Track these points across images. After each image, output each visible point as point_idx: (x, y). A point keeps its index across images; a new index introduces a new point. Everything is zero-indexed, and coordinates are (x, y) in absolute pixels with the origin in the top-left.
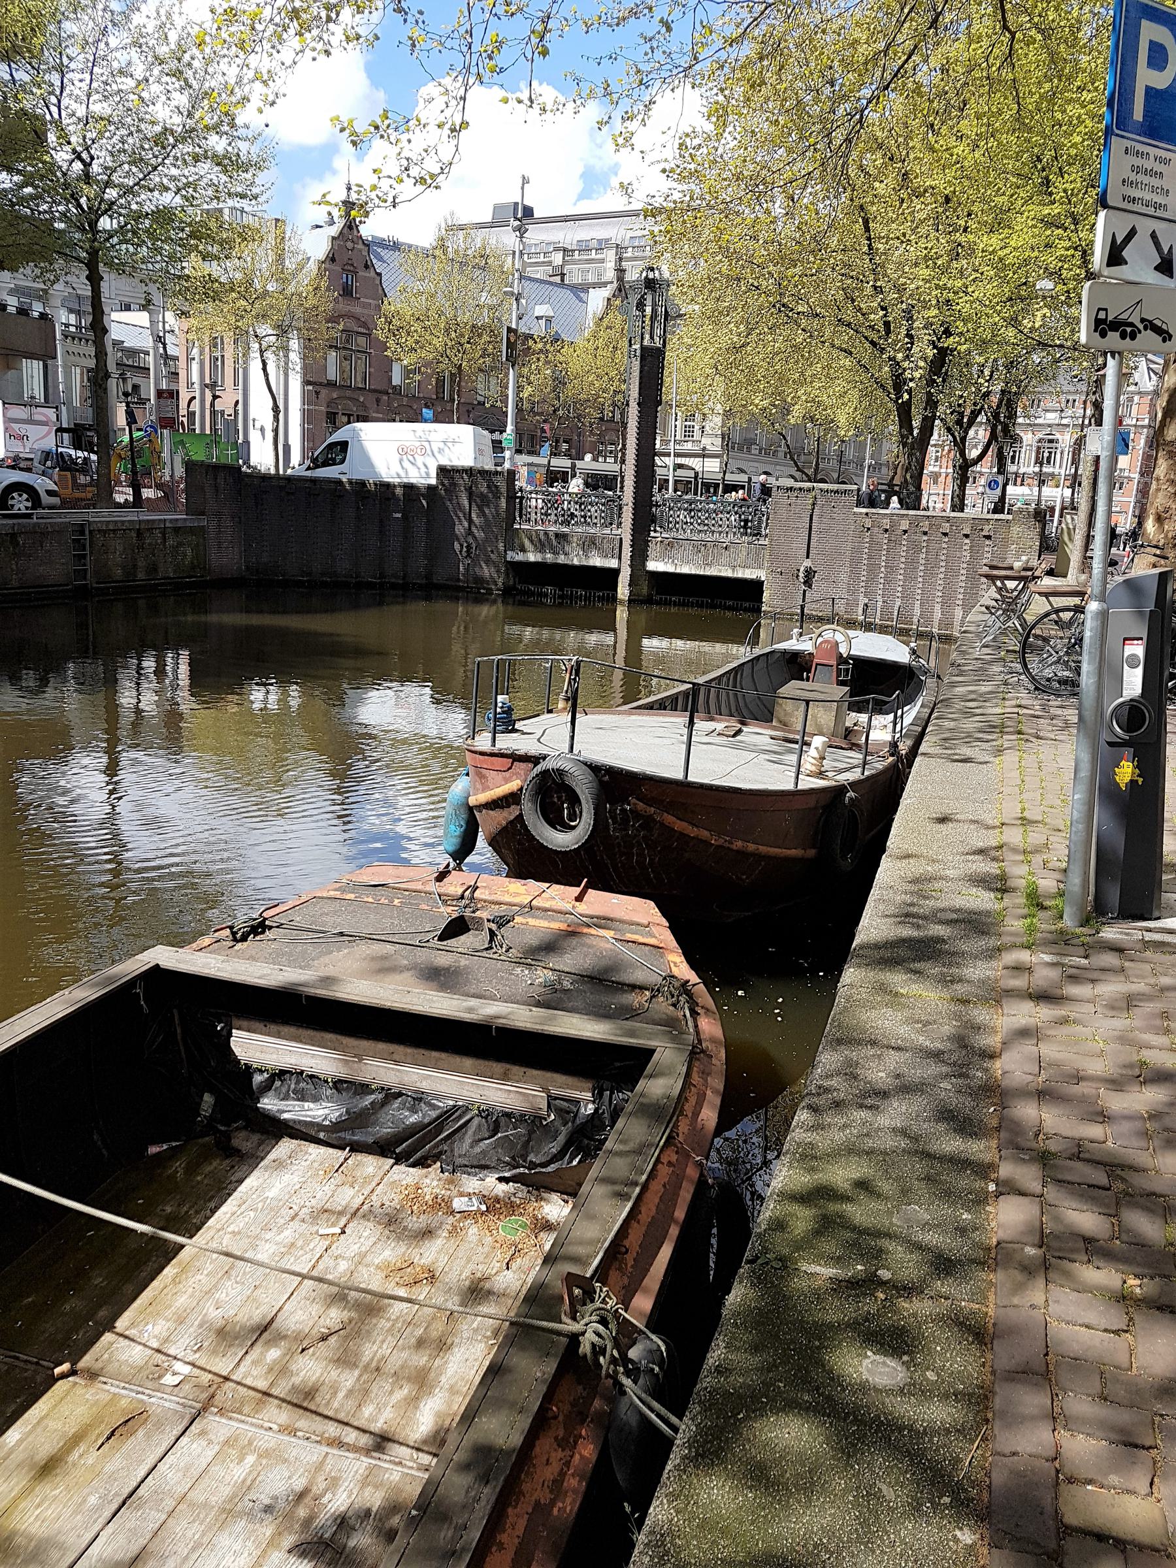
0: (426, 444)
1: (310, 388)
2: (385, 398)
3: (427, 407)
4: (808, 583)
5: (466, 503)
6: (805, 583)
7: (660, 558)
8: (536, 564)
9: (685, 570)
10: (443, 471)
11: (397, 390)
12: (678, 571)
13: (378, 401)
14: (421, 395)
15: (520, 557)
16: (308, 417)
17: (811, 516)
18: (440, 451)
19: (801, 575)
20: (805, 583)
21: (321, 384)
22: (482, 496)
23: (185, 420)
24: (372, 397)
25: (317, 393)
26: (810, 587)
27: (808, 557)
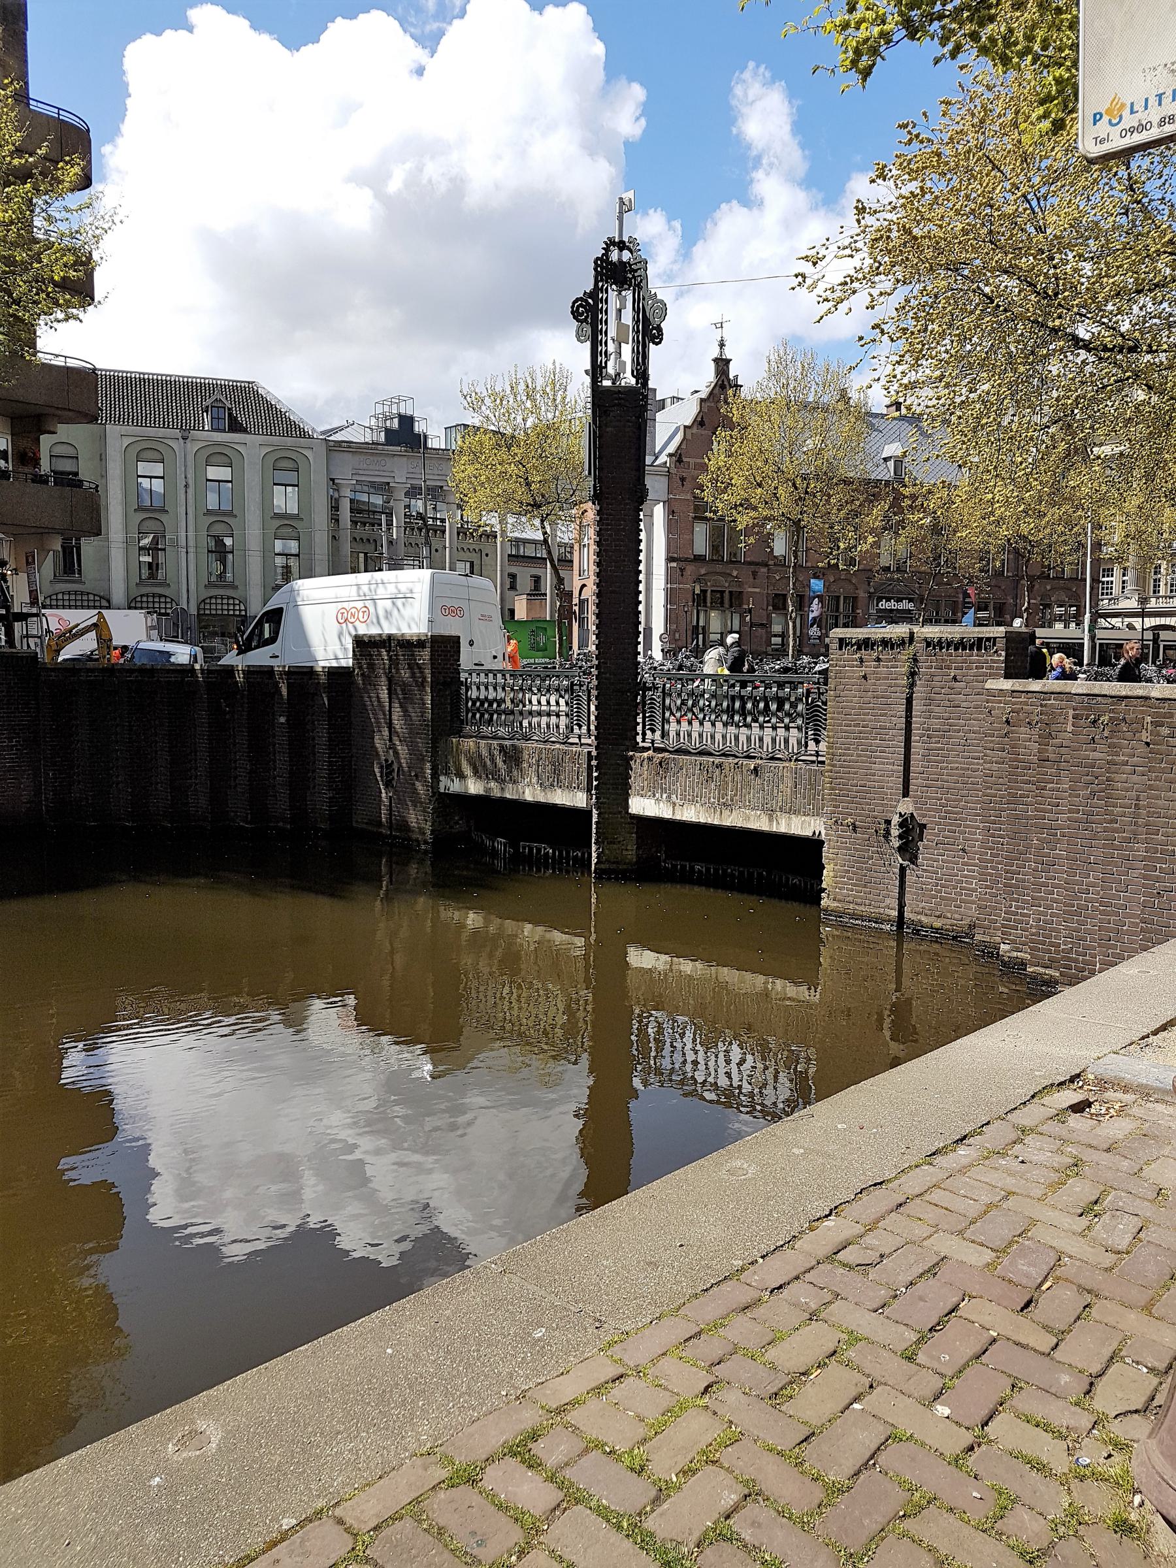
0: (369, 604)
1: (674, 564)
2: (764, 570)
3: (816, 577)
4: (908, 849)
5: (384, 695)
6: (901, 849)
7: (652, 791)
8: (477, 798)
9: (690, 814)
10: (364, 646)
11: (781, 563)
12: (678, 817)
13: (755, 574)
14: (809, 564)
15: (455, 786)
16: (671, 596)
17: (909, 701)
18: (388, 615)
19: (895, 832)
20: (901, 849)
21: (686, 560)
22: (404, 686)
23: (576, 608)
24: (747, 571)
25: (682, 570)
26: (913, 859)
27: (906, 794)
